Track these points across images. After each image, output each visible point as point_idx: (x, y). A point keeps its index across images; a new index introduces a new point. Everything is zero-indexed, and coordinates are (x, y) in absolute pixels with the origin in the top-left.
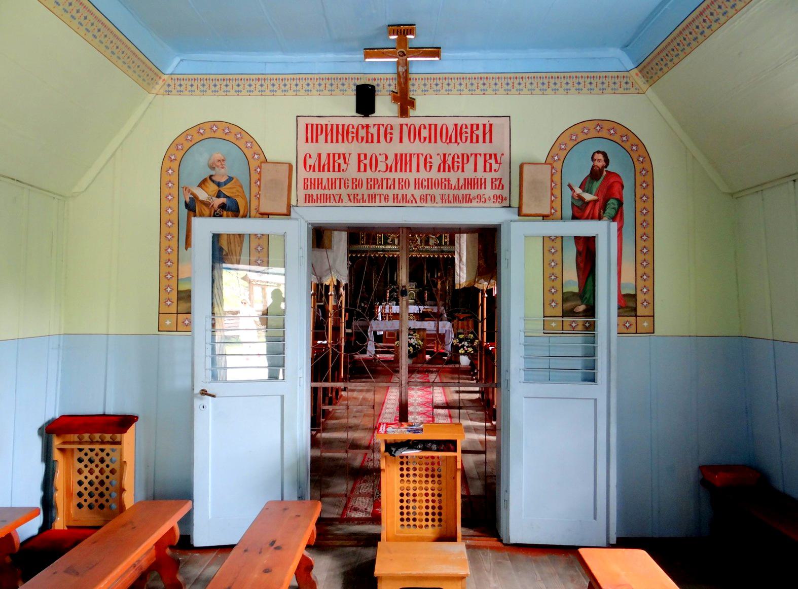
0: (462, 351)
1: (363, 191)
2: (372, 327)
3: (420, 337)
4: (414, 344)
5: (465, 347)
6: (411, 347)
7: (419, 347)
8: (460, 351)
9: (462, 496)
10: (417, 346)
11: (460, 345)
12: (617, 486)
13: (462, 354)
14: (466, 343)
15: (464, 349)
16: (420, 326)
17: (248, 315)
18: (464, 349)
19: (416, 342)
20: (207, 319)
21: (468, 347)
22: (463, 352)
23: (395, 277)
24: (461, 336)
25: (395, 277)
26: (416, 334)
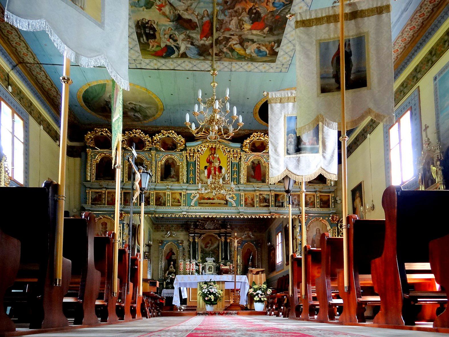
0: (257, 298)
1: (235, 169)
2: (177, 280)
3: (219, 287)
4: (214, 292)
5: (259, 295)
6: (212, 296)
7: (219, 295)
8: (255, 299)
9: (74, 324)
10: (217, 295)
11: (255, 294)
12: (84, 311)
13: (256, 301)
14: (259, 292)
15: (258, 296)
16: (220, 279)
17: (402, 138)
18: (258, 296)
19: (217, 291)
20: (139, 87)
21: (261, 295)
22: (258, 299)
23: (130, 263)
24: (256, 287)
25: (130, 263)
26: (216, 285)
